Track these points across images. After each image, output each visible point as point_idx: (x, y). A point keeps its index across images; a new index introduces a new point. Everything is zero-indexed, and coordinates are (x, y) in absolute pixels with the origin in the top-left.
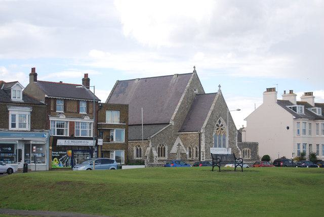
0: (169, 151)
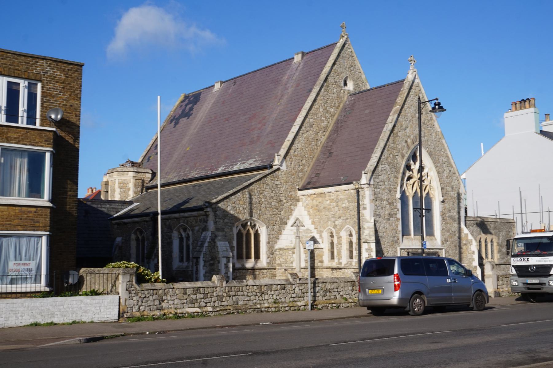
0: (271, 243)
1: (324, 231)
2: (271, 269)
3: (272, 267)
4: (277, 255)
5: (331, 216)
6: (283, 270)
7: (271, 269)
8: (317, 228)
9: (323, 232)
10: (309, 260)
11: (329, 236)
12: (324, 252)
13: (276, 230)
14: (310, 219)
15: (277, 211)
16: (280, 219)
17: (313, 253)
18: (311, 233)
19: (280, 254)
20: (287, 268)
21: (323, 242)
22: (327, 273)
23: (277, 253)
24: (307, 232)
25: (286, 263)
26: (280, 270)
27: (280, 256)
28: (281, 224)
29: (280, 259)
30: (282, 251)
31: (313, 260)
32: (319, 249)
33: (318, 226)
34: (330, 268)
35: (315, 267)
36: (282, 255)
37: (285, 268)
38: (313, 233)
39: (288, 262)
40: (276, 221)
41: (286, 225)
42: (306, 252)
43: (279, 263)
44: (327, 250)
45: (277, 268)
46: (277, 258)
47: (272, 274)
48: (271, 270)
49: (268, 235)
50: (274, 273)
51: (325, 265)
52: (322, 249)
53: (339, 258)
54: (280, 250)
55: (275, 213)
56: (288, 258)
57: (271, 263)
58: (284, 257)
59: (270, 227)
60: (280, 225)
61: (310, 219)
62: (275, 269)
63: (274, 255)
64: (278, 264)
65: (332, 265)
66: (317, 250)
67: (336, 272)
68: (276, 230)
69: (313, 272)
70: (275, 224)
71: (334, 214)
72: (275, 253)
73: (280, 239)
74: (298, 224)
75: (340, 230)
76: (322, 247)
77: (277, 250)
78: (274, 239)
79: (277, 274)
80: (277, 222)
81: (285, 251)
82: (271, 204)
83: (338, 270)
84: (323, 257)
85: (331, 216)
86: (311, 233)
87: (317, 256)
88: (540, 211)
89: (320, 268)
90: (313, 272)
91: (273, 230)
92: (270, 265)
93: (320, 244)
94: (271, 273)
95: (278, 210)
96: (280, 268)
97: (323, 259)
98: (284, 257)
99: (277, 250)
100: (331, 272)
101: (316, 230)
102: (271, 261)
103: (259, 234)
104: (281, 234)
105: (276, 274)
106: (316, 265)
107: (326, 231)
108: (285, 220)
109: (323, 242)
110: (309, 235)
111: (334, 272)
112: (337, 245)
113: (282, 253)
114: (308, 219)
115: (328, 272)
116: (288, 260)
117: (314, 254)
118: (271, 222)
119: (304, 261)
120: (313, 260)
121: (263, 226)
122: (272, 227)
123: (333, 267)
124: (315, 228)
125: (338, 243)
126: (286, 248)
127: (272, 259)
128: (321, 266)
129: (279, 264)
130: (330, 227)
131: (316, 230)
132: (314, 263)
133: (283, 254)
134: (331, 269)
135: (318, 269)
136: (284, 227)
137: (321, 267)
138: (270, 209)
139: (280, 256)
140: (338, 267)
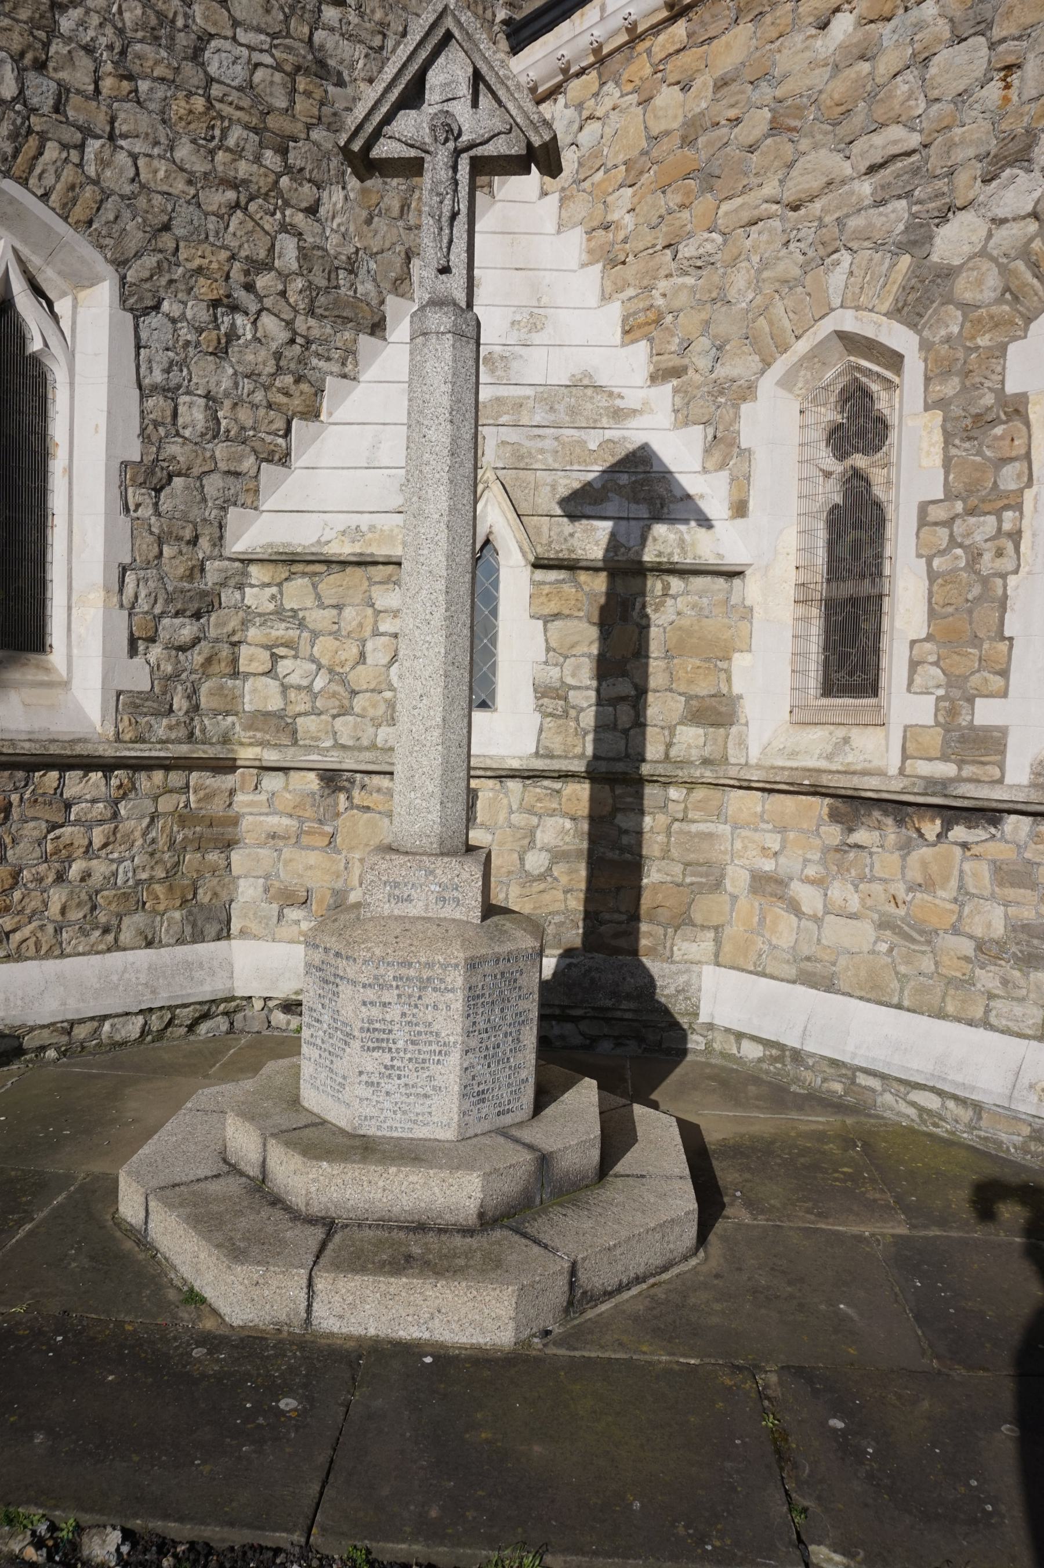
1: (767, 385)
2: (167, 765)
3: (183, 750)
4: (249, 617)
5: (865, 188)
6: (311, 782)
7: (167, 765)
8: (677, 372)
9: (748, 392)
10: (585, 699)
11: (818, 435)
12: (747, 613)
13: (260, 358)
14: (605, 298)
15: (270, 158)
16: (304, 254)
17: (625, 618)
18: (619, 415)
19: (279, 613)
20: (349, 764)
21: (740, 509)
22: (773, 842)
23: (256, 598)
24: (573, 411)
25: (345, 711)
26: (272, 782)
27: (280, 631)
28: (311, 312)
29: (284, 667)
30: (300, 582)
31: (624, 688)
32: (699, 582)
33: (686, 346)
34: (815, 791)
35: (646, 769)
36: (302, 625)
37: (332, 760)
38: (634, 423)
39: (359, 703)
40: (266, 266)
41: (365, 341)
42: (552, 607)
43: (275, 704)
44: (790, 592)
45: (246, 754)
46: (254, 660)
47: (184, 818)
48: (176, 778)
49: (144, 391)
50: (216, 808)
51: (754, 754)
52: (733, 574)
53: (954, 681)
54: (283, 572)
55: (243, 169)
56: (362, 656)
57: (180, 703)
58: (324, 647)
59: (166, 306)
60: (301, 324)
61: (605, 298)
62: (226, 766)
63: (216, 625)
64: (262, 718)
65: (851, 758)
66: (676, 583)
67: (905, 848)
68: (260, 358)
69: (623, 821)
70: (240, 294)
71: (914, 140)
72: (229, 596)
73: (298, 461)
74: (461, 110)
75: (997, 323)
76: (733, 558)
77: (256, 572)
78: (221, 450)
79: (246, 823)
80: (264, 281)
81: (332, 584)
82: (196, 55)
83: (932, 828)
84: (740, 662)
85: (865, 188)
86: (619, 415)
87: (668, 655)
88: (475, 768)
89: (691, 785)
90: (623, 821)
91: (221, 351)
92: (161, 728)
93: (705, 522)
94: (166, 804)
95: (283, 152)
96: (271, 757)
97: (738, 687)
98: (324, 647)
99: (256, 572)
100: (833, 833)
101: (667, 388)
102: (175, 676)
103: (35, 360)
104: (312, 413)
105: (235, 821)
106: (653, 750)
107: (786, 382)
108: (365, 288)
109: (740, 509)
110: (593, 440)
111: (861, 836)
112: (937, 513)
113: (309, 602)
114: (593, 299)
115: (782, 830)
116: (361, 677)
117: (643, 628)
118: (191, 257)
119: (527, 697)
120: (624, 688)
121: (82, 281)
122: (196, 311)
123: (870, 785)
124: (659, 376)
125: (950, 496)
126: (345, 549)
127: (197, 657)
128: (706, 762)
129: (267, 714)
130: (849, 322)
131: (665, 392)
132: (640, 724)
133: (321, 619)
134: (821, 806)
135: (674, 793)
136: (350, 352)
137: (709, 775)
138: (178, 107)
139: (280, 631)
140: (933, 784)
